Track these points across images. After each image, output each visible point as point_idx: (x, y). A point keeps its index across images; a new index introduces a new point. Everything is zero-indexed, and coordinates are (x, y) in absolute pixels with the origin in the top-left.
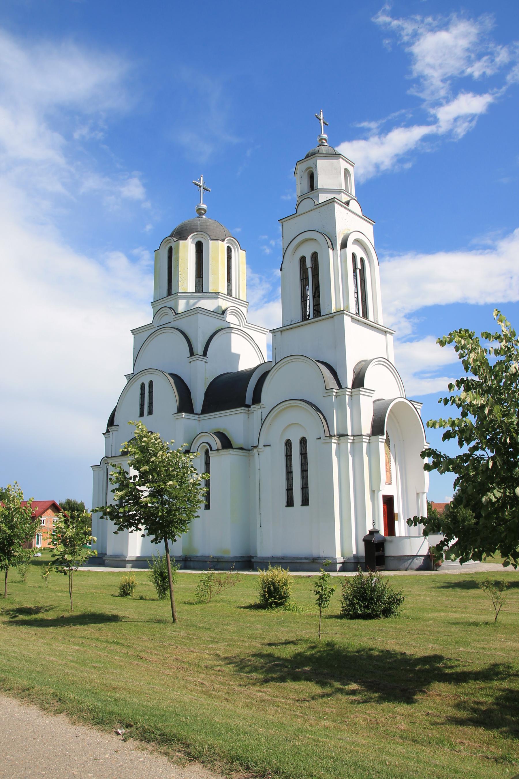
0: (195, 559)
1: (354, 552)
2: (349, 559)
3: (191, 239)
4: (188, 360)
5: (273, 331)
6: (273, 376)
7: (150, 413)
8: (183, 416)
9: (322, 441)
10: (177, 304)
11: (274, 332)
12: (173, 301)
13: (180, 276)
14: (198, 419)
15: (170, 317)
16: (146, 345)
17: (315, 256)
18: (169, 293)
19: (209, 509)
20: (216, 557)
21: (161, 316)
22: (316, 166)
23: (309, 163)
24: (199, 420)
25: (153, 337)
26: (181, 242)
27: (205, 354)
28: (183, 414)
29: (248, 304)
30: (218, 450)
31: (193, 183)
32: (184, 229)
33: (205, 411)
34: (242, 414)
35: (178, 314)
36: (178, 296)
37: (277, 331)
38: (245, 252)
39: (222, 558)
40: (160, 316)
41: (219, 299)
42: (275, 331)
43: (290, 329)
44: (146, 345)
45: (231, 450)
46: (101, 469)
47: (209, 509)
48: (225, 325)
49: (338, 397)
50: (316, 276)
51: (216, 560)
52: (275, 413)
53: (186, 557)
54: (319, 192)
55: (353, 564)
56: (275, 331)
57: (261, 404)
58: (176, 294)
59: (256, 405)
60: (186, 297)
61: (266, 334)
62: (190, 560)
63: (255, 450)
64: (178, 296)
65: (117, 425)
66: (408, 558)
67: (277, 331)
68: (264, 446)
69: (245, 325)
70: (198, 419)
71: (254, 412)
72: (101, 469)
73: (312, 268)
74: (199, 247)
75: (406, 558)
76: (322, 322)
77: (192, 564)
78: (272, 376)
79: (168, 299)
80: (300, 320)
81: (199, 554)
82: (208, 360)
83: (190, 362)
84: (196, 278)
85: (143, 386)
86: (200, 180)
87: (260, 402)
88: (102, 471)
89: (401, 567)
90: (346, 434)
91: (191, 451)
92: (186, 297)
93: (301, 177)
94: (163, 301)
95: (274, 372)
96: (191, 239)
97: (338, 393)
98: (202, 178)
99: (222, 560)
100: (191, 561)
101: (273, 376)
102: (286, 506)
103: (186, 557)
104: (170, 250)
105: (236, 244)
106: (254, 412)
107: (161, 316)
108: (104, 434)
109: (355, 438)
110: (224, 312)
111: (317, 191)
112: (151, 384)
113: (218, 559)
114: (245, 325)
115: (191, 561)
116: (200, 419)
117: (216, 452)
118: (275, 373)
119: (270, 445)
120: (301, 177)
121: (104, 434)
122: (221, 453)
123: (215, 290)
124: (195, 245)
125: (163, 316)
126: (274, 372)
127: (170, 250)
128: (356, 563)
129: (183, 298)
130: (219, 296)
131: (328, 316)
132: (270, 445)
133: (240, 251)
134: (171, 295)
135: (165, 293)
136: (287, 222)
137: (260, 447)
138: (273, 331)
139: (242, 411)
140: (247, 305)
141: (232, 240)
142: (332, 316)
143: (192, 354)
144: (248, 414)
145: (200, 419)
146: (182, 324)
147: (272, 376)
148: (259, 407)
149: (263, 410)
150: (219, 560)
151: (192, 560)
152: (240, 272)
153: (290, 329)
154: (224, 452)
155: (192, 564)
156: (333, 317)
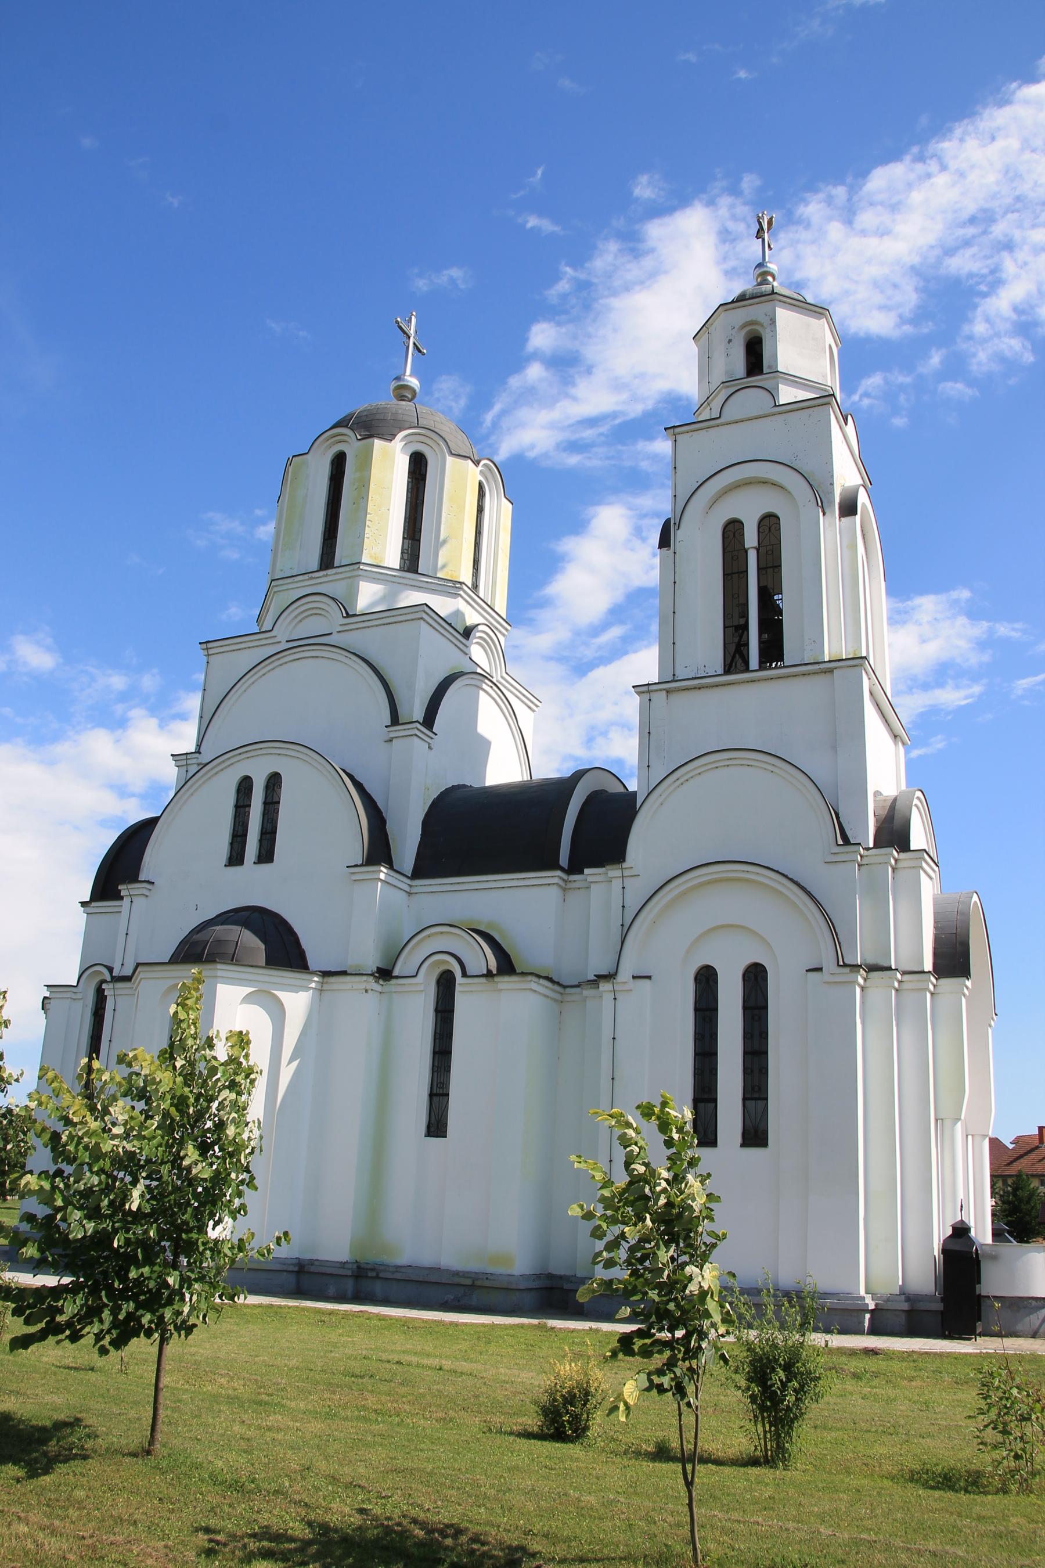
0: (393, 1273)
1: (900, 1283)
2: (888, 1300)
3: (402, 440)
4: (384, 733)
5: (645, 689)
6: (665, 799)
7: (266, 855)
8: (382, 876)
9: (825, 976)
10: (353, 593)
11: (649, 692)
12: (344, 583)
13: (368, 523)
14: (407, 889)
15: (332, 620)
16: (246, 685)
17: (769, 524)
18: (327, 560)
19: (443, 1135)
20: (468, 1272)
21: (299, 618)
22: (773, 321)
23: (754, 312)
24: (409, 894)
25: (271, 666)
26: (378, 443)
27: (429, 720)
28: (382, 869)
29: (509, 628)
30: (489, 974)
31: (397, 322)
32: (378, 417)
33: (421, 871)
34: (555, 887)
35: (355, 615)
36: (360, 573)
37: (657, 691)
38: (511, 505)
39: (487, 1276)
40: (296, 617)
41: (460, 598)
42: (652, 688)
43: (695, 688)
44: (246, 685)
45: (514, 978)
46: (79, 996)
47: (443, 1135)
48: (468, 667)
49: (862, 868)
50: (770, 571)
51: (469, 1282)
52: (676, 892)
53: (359, 1267)
54: (780, 380)
55: (903, 1317)
56: (652, 688)
57: (625, 865)
58: (356, 567)
59: (608, 867)
60: (382, 577)
61: (534, 711)
62: (374, 1274)
63: (605, 987)
64: (360, 573)
65: (148, 882)
66: (1039, 1303)
67: (657, 691)
68: (634, 977)
69: (502, 677)
70: (407, 889)
71: (592, 886)
72: (79, 996)
73: (758, 550)
74: (418, 466)
75: (1034, 1303)
76: (755, 686)
77: (378, 1288)
78: (663, 797)
79: (327, 575)
80: (720, 671)
81: (402, 1260)
82: (436, 741)
83: (391, 740)
84: (404, 538)
85: (245, 786)
86: (410, 321)
87: (624, 860)
88: (82, 1001)
89: (1019, 1327)
90: (886, 965)
91: (396, 973)
92: (382, 577)
93: (730, 341)
94: (312, 578)
95: (670, 785)
96: (402, 440)
97: (865, 859)
98: (413, 317)
99: (487, 1283)
100: (377, 1277)
101: (665, 799)
102: (742, 1145)
103: (359, 1267)
104: (339, 462)
105: (495, 481)
106: (592, 886)
107: (299, 618)
108: (84, 904)
109: (906, 977)
110: (468, 632)
111: (774, 378)
112: (274, 781)
113: (474, 1280)
114: (502, 677)
115: (377, 1277)
116: (414, 890)
117: (483, 980)
118: (676, 788)
119: (649, 977)
120: (730, 341)
121: (84, 904)
122: (501, 986)
123: (451, 576)
124: (408, 458)
125: (308, 616)
126: (670, 785)
127: (339, 462)
128: (546, 1288)
129: (375, 578)
130: (461, 593)
131: (816, 667)
132: (649, 977)
133: (504, 500)
134: (333, 567)
135: (314, 559)
136: (690, 434)
137: (620, 978)
138: (645, 689)
139: (556, 880)
140: (507, 630)
141: (490, 470)
142: (827, 669)
143: (395, 720)
144: (564, 890)
145: (414, 890)
146: (366, 640)
147: (663, 797)
148: (618, 873)
149: (628, 882)
150: (478, 1283)
151: (381, 1275)
152: (500, 551)
153: (695, 688)
154: (506, 982)
155: (378, 1288)
156: (831, 671)
